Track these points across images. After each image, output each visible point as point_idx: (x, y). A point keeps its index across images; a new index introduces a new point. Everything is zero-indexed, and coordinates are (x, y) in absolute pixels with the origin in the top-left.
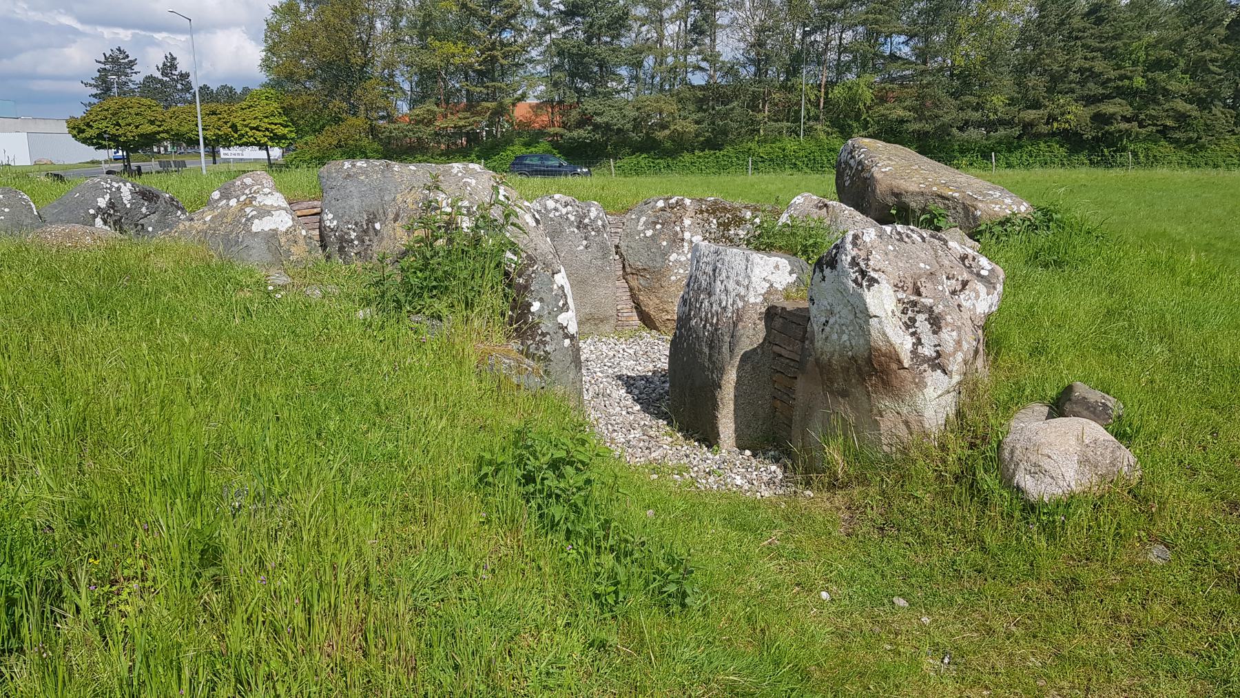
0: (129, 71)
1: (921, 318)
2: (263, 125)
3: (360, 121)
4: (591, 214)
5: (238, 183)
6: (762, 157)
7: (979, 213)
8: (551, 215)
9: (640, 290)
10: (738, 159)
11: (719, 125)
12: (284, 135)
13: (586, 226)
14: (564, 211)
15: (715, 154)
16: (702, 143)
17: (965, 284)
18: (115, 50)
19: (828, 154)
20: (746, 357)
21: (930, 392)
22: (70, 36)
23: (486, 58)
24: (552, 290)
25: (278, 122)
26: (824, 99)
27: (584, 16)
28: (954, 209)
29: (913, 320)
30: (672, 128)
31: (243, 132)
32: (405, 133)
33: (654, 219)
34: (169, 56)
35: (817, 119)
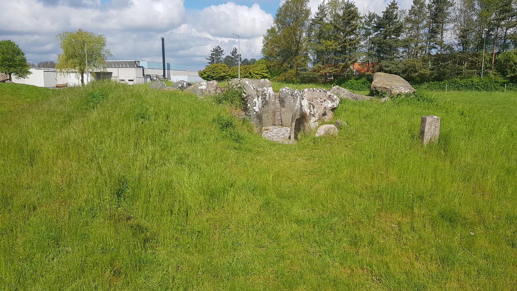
0: (221, 54)
1: (311, 106)
2: (260, 73)
3: (293, 71)
4: (295, 92)
6: (461, 85)
8: (284, 92)
11: (441, 71)
12: (267, 76)
13: (293, 95)
14: (287, 91)
15: (439, 83)
16: (434, 78)
17: (325, 100)
18: (217, 47)
19: (494, 84)
20: (297, 120)
21: (312, 121)
22: (208, 41)
23: (342, 46)
24: (253, 102)
25: (265, 72)
26: (494, 60)
27: (384, 28)
29: (310, 107)
30: (419, 72)
31: (253, 75)
32: (309, 75)
34: (235, 48)
35: (490, 68)
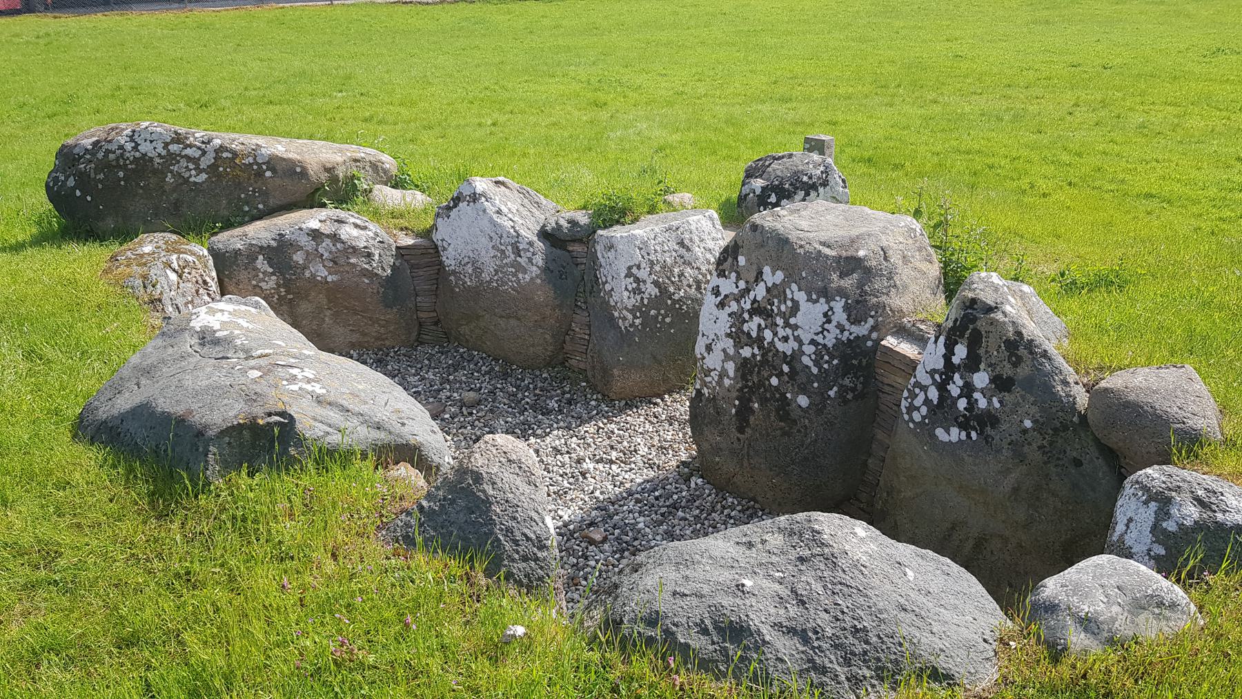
7: (388, 166)
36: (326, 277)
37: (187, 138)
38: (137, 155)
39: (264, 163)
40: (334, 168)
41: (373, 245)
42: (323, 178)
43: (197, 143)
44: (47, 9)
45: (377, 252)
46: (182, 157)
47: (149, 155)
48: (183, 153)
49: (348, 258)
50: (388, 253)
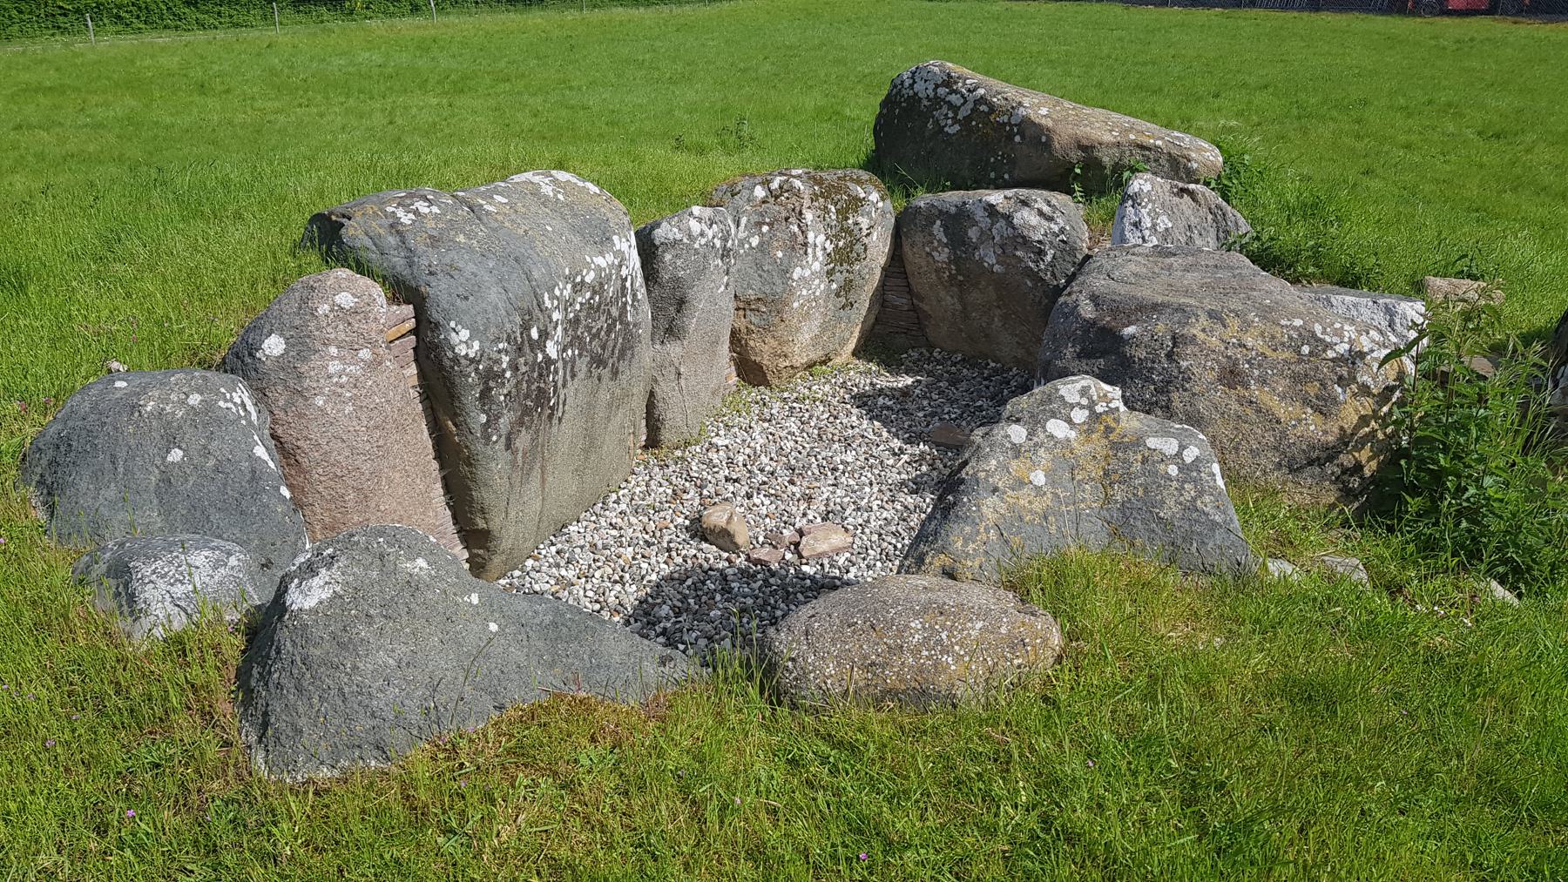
5: (324, 309)
6: (61, 8)
7: (1195, 165)
9: (749, 331)
10: (21, 12)
28: (1156, 161)
33: (755, 218)
36: (993, 265)
37: (956, 83)
38: (911, 93)
39: (1016, 125)
40: (1093, 147)
41: (1051, 243)
42: (1075, 157)
43: (963, 90)
44: (1519, 12)
45: (1050, 253)
46: (946, 103)
47: (920, 95)
48: (947, 99)
49: (1016, 249)
50: (1067, 258)
